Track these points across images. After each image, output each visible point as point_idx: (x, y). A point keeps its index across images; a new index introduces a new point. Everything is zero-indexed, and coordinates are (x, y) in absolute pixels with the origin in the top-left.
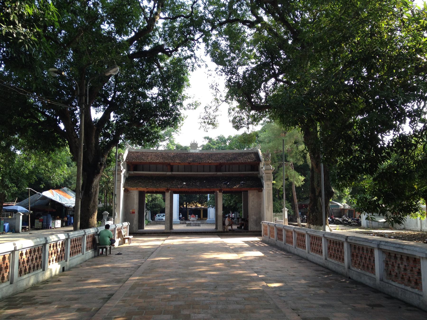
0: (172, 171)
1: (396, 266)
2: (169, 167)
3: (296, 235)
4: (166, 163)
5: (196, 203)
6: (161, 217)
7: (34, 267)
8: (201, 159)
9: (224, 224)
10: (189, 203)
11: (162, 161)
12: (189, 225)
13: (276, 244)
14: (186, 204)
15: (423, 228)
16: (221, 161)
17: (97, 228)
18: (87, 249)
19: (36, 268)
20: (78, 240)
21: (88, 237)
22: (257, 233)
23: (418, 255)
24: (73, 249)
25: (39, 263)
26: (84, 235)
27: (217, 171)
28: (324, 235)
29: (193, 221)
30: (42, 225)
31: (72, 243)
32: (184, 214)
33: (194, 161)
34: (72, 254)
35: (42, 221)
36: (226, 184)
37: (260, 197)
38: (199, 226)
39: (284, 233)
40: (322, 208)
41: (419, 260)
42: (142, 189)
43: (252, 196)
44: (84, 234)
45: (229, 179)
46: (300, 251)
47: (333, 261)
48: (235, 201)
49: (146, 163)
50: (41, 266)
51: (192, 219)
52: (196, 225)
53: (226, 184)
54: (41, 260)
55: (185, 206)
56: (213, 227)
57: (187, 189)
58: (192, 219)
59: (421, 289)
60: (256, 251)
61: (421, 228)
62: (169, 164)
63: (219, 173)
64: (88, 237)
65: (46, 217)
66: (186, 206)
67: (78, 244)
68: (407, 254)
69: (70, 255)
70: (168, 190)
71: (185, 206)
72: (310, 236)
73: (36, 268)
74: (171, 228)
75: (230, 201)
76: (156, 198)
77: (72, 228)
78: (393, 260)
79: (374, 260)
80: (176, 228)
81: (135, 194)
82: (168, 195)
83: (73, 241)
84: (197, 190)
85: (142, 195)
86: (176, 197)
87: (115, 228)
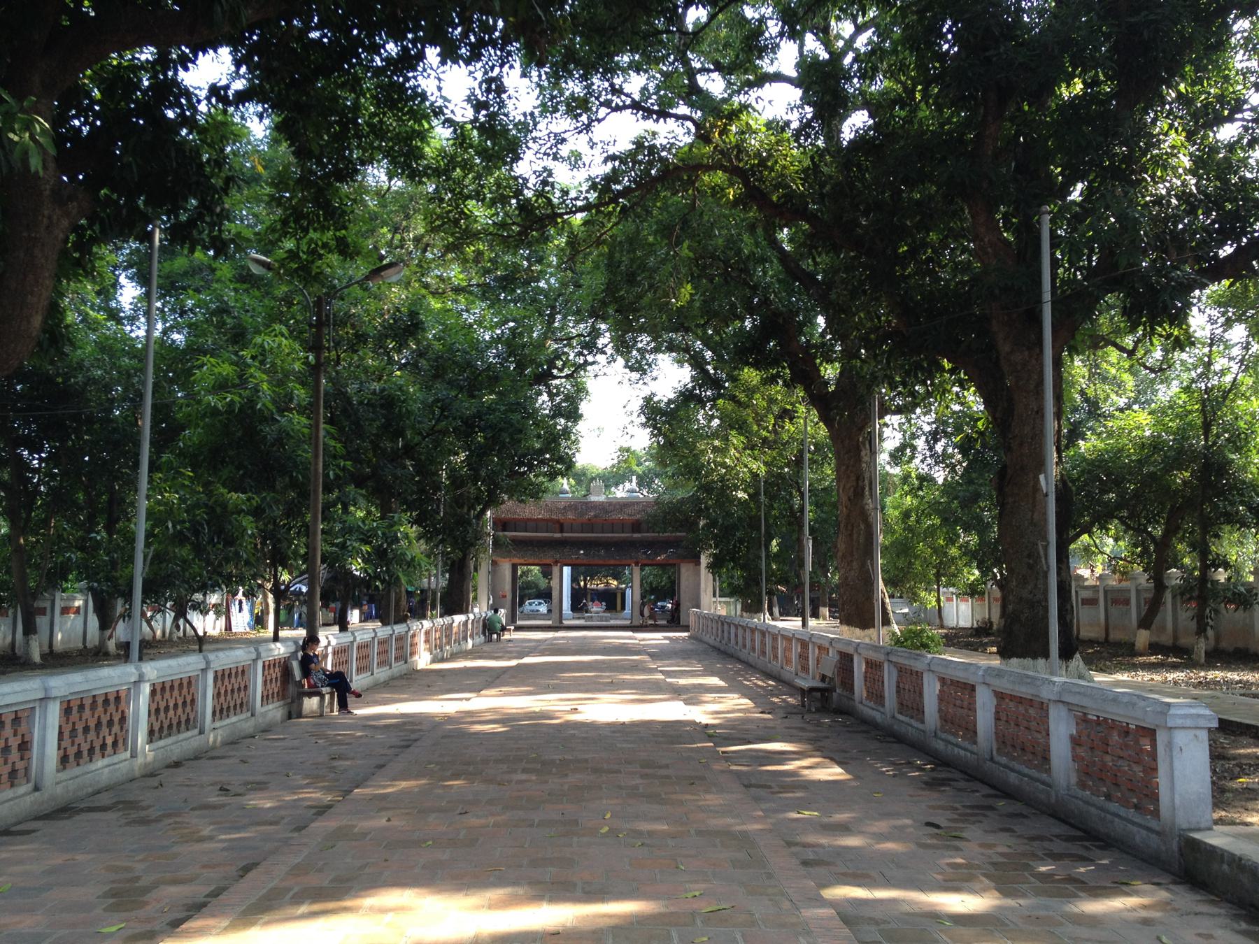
0: (562, 531)
2: (557, 526)
4: (551, 520)
5: (606, 577)
6: (534, 607)
7: (79, 754)
8: (607, 512)
9: (642, 614)
10: (592, 579)
11: (546, 516)
14: (585, 580)
18: (266, 698)
20: (172, 687)
21: (267, 667)
22: (686, 628)
23: (971, 680)
27: (633, 532)
31: (219, 682)
32: (579, 600)
33: (595, 516)
40: (530, 641)
42: (516, 561)
43: (685, 571)
44: (203, 666)
49: (520, 520)
51: (595, 609)
56: (628, 622)
58: (595, 609)
62: (558, 521)
63: (636, 535)
64: (267, 667)
67: (236, 686)
69: (214, 713)
70: (556, 563)
74: (561, 622)
76: (529, 571)
80: (566, 623)
82: (555, 570)
84: (601, 562)
85: (514, 568)
86: (567, 571)
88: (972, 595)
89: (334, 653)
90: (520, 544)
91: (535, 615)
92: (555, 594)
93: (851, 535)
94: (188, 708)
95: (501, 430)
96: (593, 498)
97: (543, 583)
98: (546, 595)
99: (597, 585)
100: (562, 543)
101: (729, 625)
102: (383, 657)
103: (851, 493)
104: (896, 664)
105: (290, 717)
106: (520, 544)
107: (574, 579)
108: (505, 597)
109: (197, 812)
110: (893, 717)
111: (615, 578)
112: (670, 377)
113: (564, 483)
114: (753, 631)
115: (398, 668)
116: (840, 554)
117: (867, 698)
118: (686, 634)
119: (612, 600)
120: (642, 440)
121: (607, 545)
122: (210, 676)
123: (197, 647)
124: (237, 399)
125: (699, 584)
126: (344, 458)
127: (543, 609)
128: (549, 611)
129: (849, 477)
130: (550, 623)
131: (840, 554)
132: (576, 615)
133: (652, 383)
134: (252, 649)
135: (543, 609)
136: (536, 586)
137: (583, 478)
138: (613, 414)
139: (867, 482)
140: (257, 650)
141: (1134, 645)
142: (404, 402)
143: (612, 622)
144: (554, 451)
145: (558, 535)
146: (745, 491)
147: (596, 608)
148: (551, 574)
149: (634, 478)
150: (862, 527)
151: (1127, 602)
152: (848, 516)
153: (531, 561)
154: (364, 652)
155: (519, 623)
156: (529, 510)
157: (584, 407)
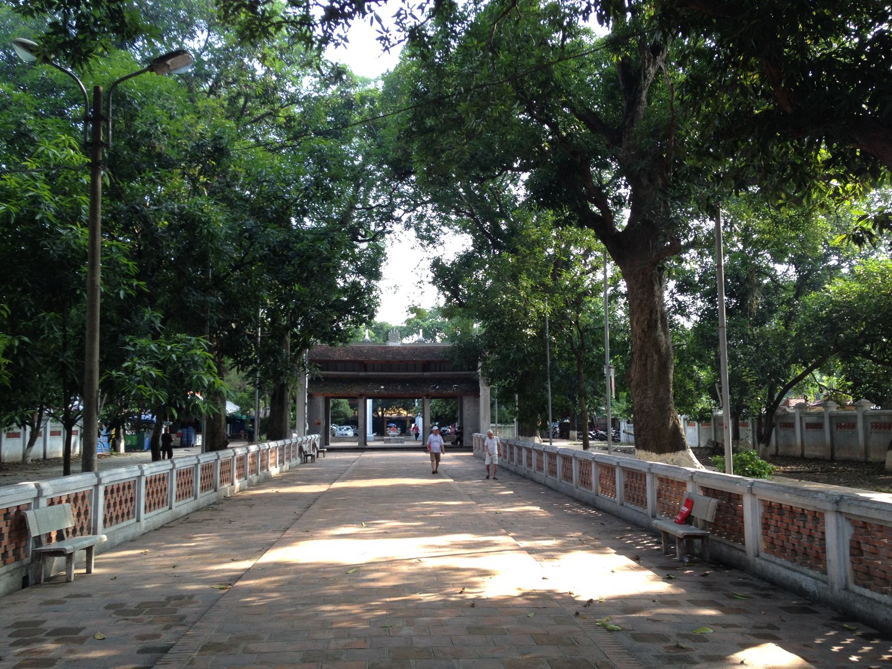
0: (366, 371)
1: (805, 532)
3: (657, 483)
5: (398, 408)
6: (343, 432)
10: (387, 409)
11: (352, 358)
12: (389, 441)
13: (594, 500)
14: (382, 411)
15: (806, 452)
16: (429, 359)
17: (97, 475)
19: (114, 520)
20: (129, 487)
22: (470, 449)
24: (112, 509)
25: (131, 509)
26: (139, 477)
27: (424, 371)
28: (649, 469)
29: (394, 436)
30: (182, 441)
32: (380, 427)
34: (179, 497)
35: (181, 436)
36: (434, 388)
37: (477, 404)
38: (402, 442)
39: (575, 466)
41: (822, 515)
43: (467, 404)
45: (439, 381)
46: (550, 480)
47: (632, 506)
48: (451, 408)
50: (134, 514)
51: (392, 433)
52: (397, 441)
53: (434, 388)
54: (89, 517)
55: (380, 413)
57: (385, 393)
58: (392, 433)
59: (744, 544)
60: (581, 545)
61: (777, 450)
62: (361, 362)
63: (426, 374)
65: (185, 430)
66: (383, 414)
68: (877, 519)
69: (105, 521)
70: (361, 396)
71: (380, 413)
72: (624, 469)
73: (114, 520)
74: (366, 444)
75: (445, 408)
77: (149, 455)
78: (776, 516)
79: (823, 539)
80: (370, 444)
81: (320, 401)
82: (361, 401)
83: (180, 474)
86: (369, 402)
87: (196, 465)
88: (699, 421)
89: (202, 469)
90: (329, 380)
91: (344, 438)
92: (361, 422)
93: (645, 365)
94: (112, 502)
95: (309, 258)
96: (391, 344)
97: (350, 413)
98: (353, 422)
99: (391, 414)
100: (366, 380)
101: (511, 447)
102: (185, 489)
103: (645, 326)
104: (849, 518)
105: (25, 583)
106: (329, 380)
107: (375, 411)
108: (319, 424)
109: (85, 591)
110: (846, 588)
111: (405, 409)
112: (456, 244)
113: (366, 334)
114: (529, 451)
115: (204, 498)
116: (633, 383)
117: (766, 551)
118: (471, 454)
119: (403, 425)
120: (433, 298)
121: (402, 381)
122: (101, 489)
123: (62, 469)
124: (14, 209)
125: (478, 413)
126: (138, 277)
127: (350, 433)
128: (356, 435)
129: (642, 310)
130: (356, 444)
131: (633, 383)
132: (377, 438)
133: (439, 248)
134: (136, 468)
135: (350, 433)
136: (345, 416)
137: (382, 331)
138: (408, 279)
139: (659, 315)
140: (140, 468)
141: (884, 463)
142: (204, 223)
143: (406, 444)
144: (360, 304)
145: (362, 374)
146: (534, 328)
147: (393, 432)
148: (357, 406)
149: (421, 331)
150: (656, 357)
151: (853, 426)
152: (642, 347)
153: (342, 393)
154: (226, 468)
155: (332, 445)
156: (339, 351)
157: (384, 269)
